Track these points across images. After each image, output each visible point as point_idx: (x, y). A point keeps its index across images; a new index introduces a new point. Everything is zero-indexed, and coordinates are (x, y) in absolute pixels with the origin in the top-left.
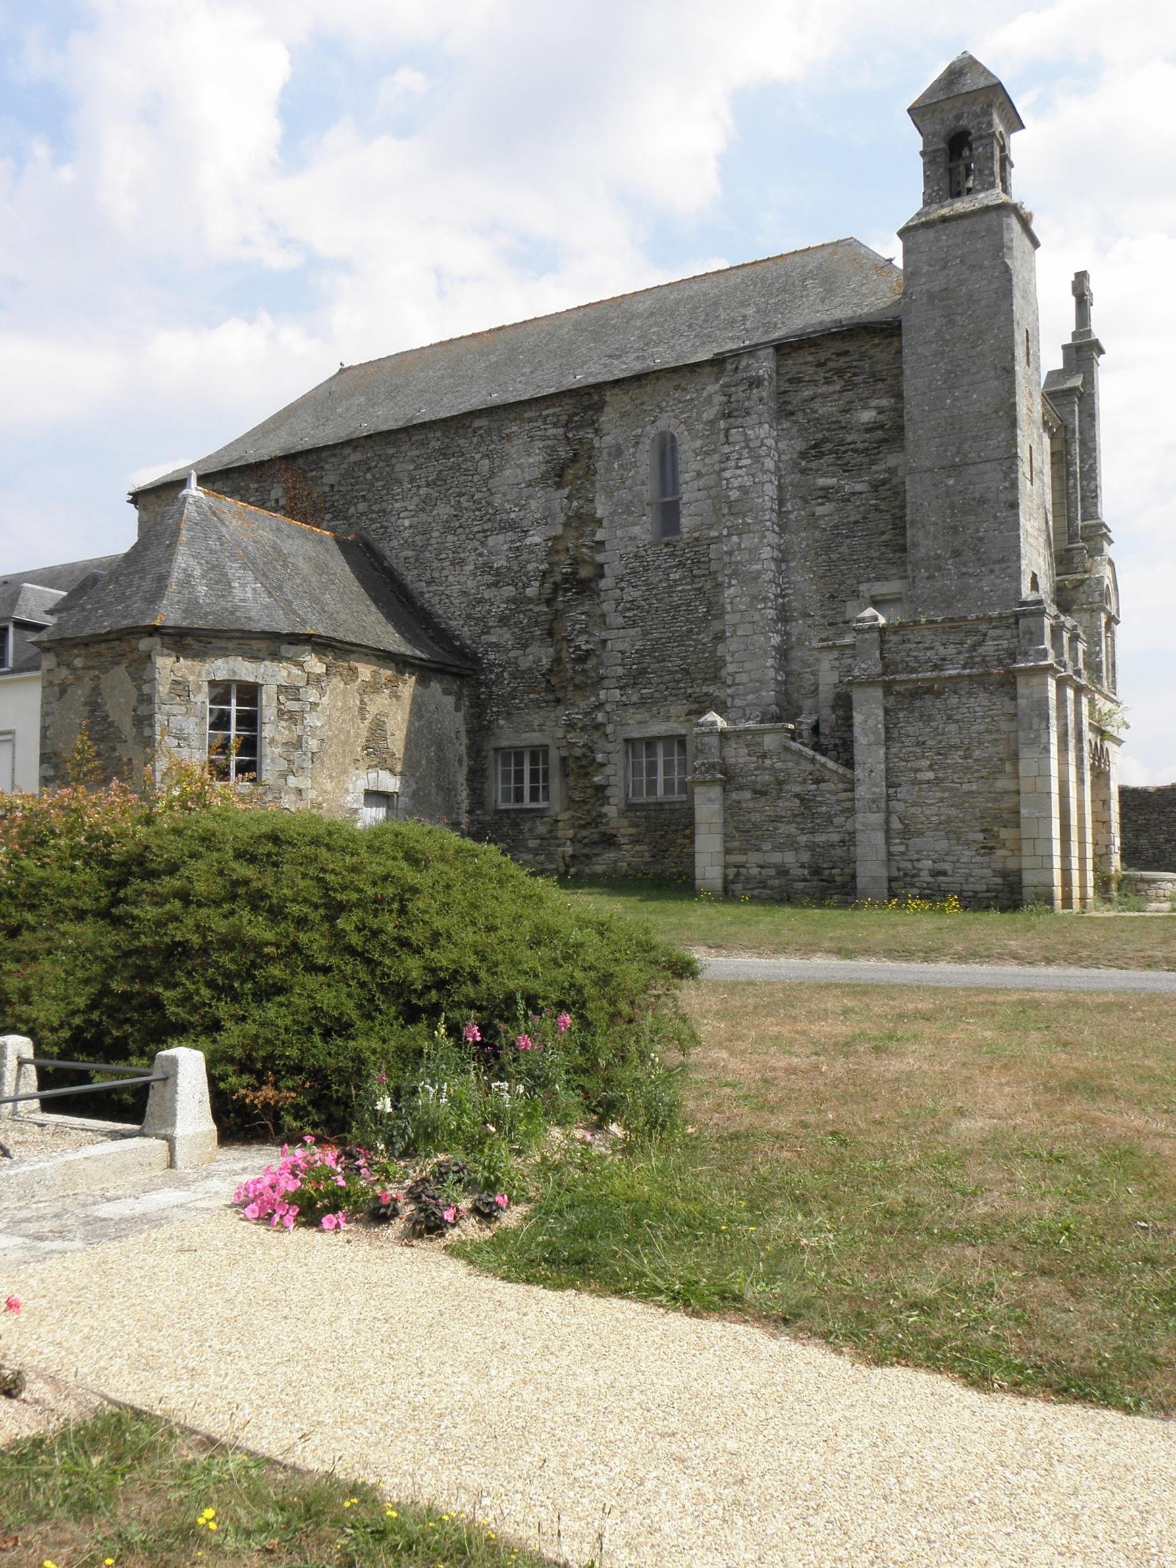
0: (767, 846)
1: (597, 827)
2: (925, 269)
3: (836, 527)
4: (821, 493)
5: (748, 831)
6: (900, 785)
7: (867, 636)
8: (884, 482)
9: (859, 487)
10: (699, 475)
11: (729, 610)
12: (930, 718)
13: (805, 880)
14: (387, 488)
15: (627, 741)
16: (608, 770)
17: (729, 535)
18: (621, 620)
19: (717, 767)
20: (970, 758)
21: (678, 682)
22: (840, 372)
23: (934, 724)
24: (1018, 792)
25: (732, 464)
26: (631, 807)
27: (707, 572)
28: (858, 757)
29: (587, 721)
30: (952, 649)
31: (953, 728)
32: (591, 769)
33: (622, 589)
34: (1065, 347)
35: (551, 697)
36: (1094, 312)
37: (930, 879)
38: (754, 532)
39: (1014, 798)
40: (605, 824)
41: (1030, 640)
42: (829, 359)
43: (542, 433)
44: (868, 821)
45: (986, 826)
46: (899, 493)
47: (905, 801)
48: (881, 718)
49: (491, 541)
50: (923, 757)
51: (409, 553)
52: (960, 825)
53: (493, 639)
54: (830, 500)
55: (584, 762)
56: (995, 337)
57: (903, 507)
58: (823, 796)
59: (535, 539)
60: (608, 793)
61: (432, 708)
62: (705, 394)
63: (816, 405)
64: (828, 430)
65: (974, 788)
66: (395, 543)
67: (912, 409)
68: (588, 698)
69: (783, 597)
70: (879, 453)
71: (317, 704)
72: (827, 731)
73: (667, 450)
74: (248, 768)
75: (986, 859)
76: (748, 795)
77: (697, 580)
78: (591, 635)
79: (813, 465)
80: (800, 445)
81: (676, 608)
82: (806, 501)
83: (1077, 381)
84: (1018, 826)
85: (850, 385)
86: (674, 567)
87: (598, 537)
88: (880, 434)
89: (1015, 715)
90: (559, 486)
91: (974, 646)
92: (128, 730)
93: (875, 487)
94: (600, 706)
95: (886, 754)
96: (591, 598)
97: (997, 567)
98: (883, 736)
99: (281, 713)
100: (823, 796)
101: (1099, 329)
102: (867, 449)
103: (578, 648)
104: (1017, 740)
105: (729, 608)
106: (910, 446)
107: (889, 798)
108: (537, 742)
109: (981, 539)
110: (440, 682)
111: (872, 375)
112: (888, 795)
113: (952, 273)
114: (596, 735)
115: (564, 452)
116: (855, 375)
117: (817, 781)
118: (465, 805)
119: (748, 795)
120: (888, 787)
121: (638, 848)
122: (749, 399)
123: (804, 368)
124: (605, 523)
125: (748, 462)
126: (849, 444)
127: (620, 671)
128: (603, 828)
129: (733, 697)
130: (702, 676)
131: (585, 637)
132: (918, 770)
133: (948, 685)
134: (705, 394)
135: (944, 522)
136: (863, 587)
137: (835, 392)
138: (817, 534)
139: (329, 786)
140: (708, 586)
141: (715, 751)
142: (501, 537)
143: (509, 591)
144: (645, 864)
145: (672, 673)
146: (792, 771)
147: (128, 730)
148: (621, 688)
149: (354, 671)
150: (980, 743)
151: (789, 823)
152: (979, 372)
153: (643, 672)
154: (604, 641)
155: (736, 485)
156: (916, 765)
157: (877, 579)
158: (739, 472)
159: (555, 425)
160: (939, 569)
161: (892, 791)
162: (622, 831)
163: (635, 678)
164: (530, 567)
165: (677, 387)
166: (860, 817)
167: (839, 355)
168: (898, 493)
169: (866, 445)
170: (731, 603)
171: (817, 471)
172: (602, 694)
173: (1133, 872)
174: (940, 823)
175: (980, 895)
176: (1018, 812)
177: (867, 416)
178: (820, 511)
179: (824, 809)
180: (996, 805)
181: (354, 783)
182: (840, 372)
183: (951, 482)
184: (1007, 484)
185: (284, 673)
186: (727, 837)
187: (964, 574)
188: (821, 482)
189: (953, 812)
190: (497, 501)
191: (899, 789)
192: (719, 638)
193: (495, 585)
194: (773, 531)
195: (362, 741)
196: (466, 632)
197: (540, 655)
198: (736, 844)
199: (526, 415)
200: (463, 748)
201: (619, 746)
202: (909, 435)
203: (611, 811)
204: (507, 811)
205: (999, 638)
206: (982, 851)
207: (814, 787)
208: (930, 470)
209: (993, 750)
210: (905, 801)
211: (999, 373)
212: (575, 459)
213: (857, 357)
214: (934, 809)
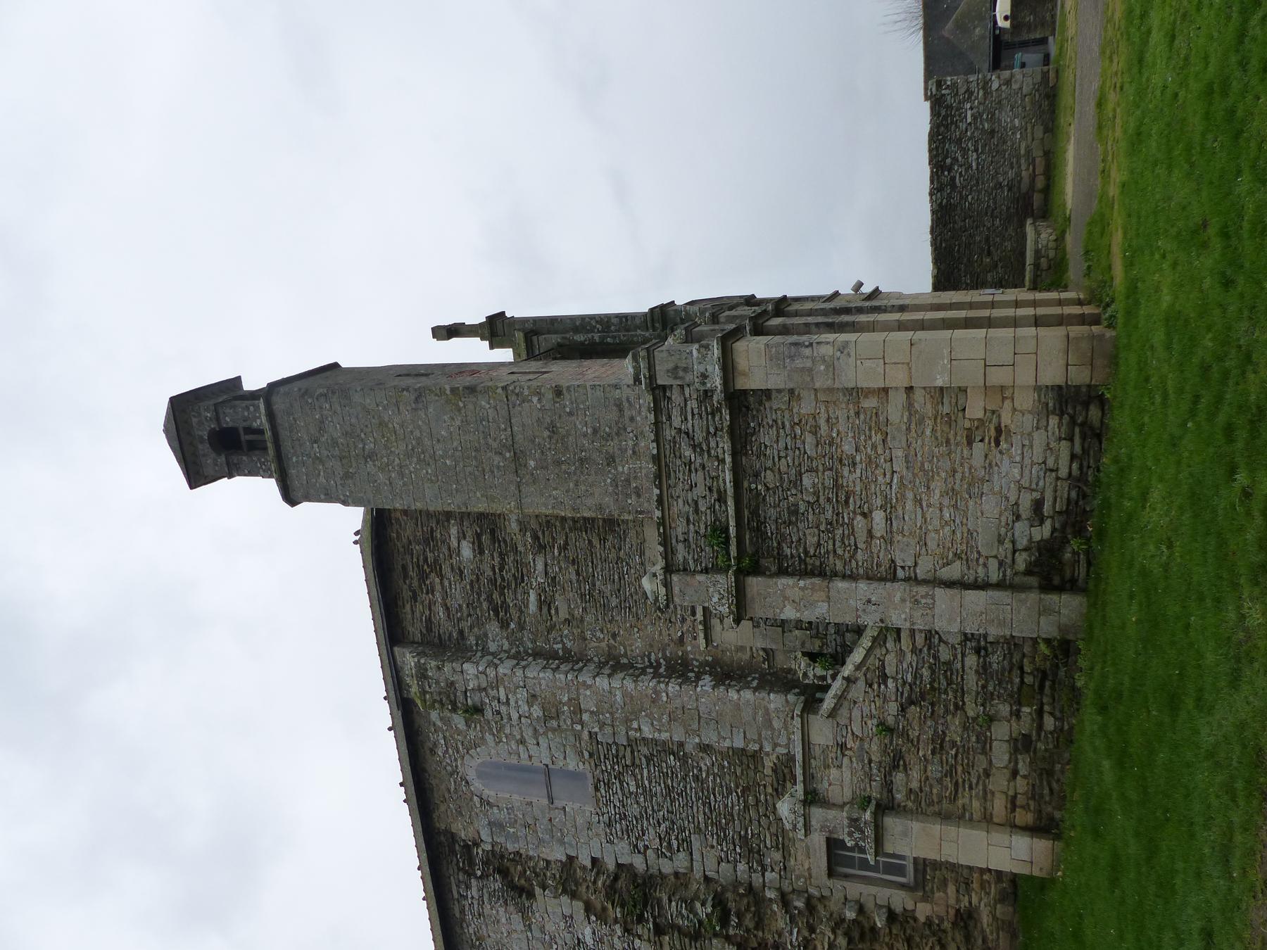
1: (944, 931)
3: (582, 596)
4: (545, 610)
5: (957, 784)
6: (893, 561)
7: (676, 590)
8: (535, 537)
9: (540, 566)
11: (668, 734)
12: (794, 511)
13: (1040, 712)
18: (682, 855)
19: (855, 816)
20: (854, 458)
21: (758, 801)
22: (423, 577)
23: (802, 508)
24: (910, 389)
25: (503, 709)
27: (629, 750)
28: (849, 619)
29: (801, 922)
31: (807, 481)
32: (866, 925)
33: (646, 847)
34: (492, 347)
36: (470, 321)
37: (1048, 525)
38: (578, 694)
39: (919, 396)
40: (941, 920)
41: (685, 370)
42: (410, 586)
43: (475, 902)
46: (548, 523)
47: (917, 556)
48: (790, 581)
50: (851, 525)
52: (958, 476)
55: (856, 935)
57: (564, 519)
58: (905, 671)
60: (899, 910)
62: (439, 723)
63: (453, 604)
64: (479, 595)
65: (900, 453)
67: (452, 504)
69: (659, 665)
70: (505, 541)
72: (818, 643)
75: (1016, 439)
76: (899, 777)
77: (637, 762)
78: (696, 897)
81: (669, 790)
83: (519, 336)
84: (963, 390)
85: (436, 567)
86: (621, 785)
87: (588, 864)
89: (791, 391)
90: (531, 895)
91: (694, 447)
93: (541, 548)
95: (844, 577)
97: (627, 413)
98: (817, 581)
100: (905, 671)
101: (477, 318)
102: (501, 554)
104: (830, 390)
107: (913, 580)
109: (595, 431)
112: (907, 579)
113: (326, 453)
115: (496, 884)
116: (426, 560)
117: (884, 678)
119: (899, 777)
120: (894, 579)
121: (975, 885)
122: (437, 683)
123: (418, 614)
125: (502, 690)
126: (495, 573)
127: (742, 867)
128: (947, 925)
129: (776, 745)
130: (751, 774)
132: (870, 532)
133: (746, 484)
134: (439, 723)
135: (575, 473)
137: (442, 583)
140: (645, 751)
141: (831, 813)
145: (746, 807)
146: (866, 710)
148: (764, 870)
151: (946, 724)
152: (419, 427)
153: (744, 840)
154: (707, 879)
155: (526, 708)
156: (861, 536)
157: (642, 554)
158: (512, 702)
159: (468, 887)
160: (628, 481)
161: (900, 574)
162: (952, 901)
163: (752, 853)
166: (940, 625)
167: (406, 576)
168: (548, 522)
169: (495, 555)
170: (660, 731)
171: (521, 612)
174: (955, 507)
175: (1078, 449)
176: (941, 389)
177: (467, 551)
179: (925, 672)
180: (929, 423)
183: (532, 463)
184: (535, 399)
187: (634, 452)
188: (533, 607)
189: (938, 486)
191: (899, 563)
194: (580, 670)
199: (458, 915)
202: (481, 507)
203: (923, 911)
205: (683, 412)
206: (1004, 445)
207: (890, 683)
210: (917, 556)
211: (420, 406)
213: (408, 557)
214: (932, 513)
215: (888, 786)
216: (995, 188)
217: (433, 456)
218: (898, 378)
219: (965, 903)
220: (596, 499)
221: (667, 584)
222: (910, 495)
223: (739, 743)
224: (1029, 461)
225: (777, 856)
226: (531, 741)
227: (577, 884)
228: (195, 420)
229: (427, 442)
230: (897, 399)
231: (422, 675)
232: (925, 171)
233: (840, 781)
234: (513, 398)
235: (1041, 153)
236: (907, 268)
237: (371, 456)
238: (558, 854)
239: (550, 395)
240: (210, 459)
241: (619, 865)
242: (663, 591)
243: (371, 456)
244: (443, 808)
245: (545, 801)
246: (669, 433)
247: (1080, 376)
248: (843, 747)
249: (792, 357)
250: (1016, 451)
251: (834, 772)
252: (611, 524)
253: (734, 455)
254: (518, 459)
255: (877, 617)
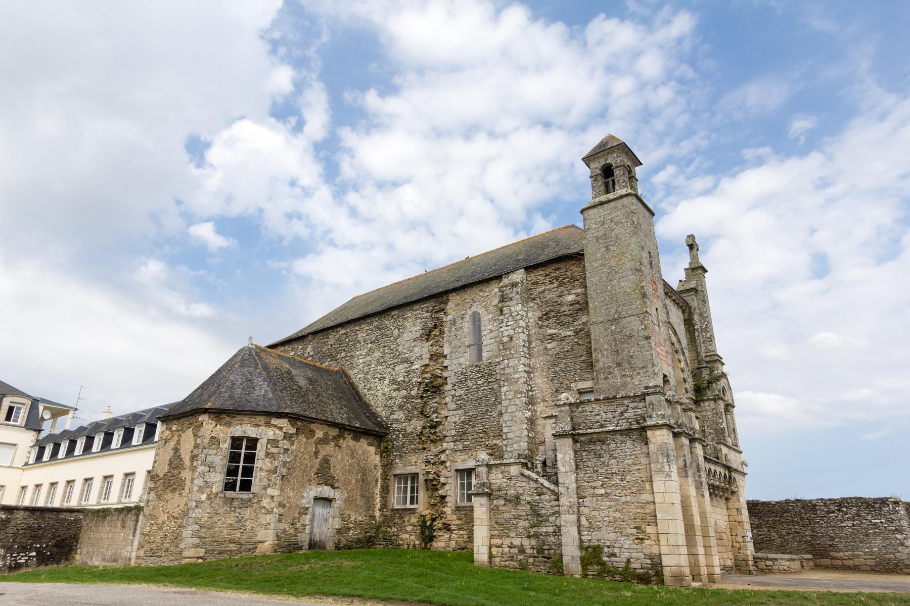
0: (513, 534)
2: (594, 226)
7: (563, 409)
8: (581, 330)
9: (568, 333)
10: (491, 331)
12: (600, 456)
14: (354, 345)
15: (457, 471)
16: (447, 487)
17: (503, 360)
18: (455, 406)
22: (556, 278)
24: (654, 502)
25: (504, 324)
26: (458, 509)
28: (560, 480)
29: (436, 459)
30: (610, 415)
31: (613, 461)
34: (685, 270)
35: (421, 446)
39: (652, 506)
44: (567, 519)
45: (638, 524)
48: (572, 456)
49: (397, 368)
51: (361, 376)
53: (395, 417)
54: (554, 341)
55: (434, 483)
56: (631, 254)
57: (590, 343)
59: (416, 366)
61: (360, 452)
65: (629, 499)
66: (355, 371)
67: (591, 292)
68: (437, 447)
71: (288, 450)
73: (476, 320)
74: (246, 486)
75: (639, 546)
76: (502, 502)
79: (545, 323)
80: (538, 314)
82: (542, 342)
83: (693, 284)
85: (562, 284)
88: (577, 306)
89: (648, 454)
90: (427, 340)
91: (622, 413)
92: (187, 462)
93: (577, 333)
94: (443, 451)
96: (440, 395)
97: (641, 371)
98: (574, 467)
99: (267, 455)
103: (432, 420)
105: (503, 397)
106: (591, 311)
108: (414, 471)
109: (631, 357)
110: (367, 439)
111: (572, 278)
114: (442, 467)
115: (430, 324)
118: (378, 506)
121: (461, 532)
124: (448, 357)
127: (454, 432)
129: (506, 446)
131: (436, 415)
132: (595, 488)
136: (573, 385)
138: (548, 358)
139: (291, 494)
141: (485, 476)
142: (401, 366)
143: (404, 393)
144: (465, 542)
147: (187, 462)
149: (313, 432)
150: (630, 471)
153: (464, 433)
156: (593, 484)
157: (580, 380)
159: (427, 312)
161: (581, 500)
163: (461, 436)
164: (413, 380)
165: (481, 290)
166: (563, 517)
172: (445, 444)
173: (760, 555)
177: (571, 298)
178: (549, 346)
180: (642, 511)
181: (308, 493)
182: (556, 278)
183: (613, 328)
185: (272, 433)
186: (491, 528)
189: (618, 515)
190: (400, 348)
192: (501, 414)
193: (397, 390)
195: (314, 470)
196: (382, 412)
197: (417, 424)
198: (496, 532)
200: (379, 474)
201: (453, 474)
202: (591, 305)
203: (448, 510)
204: (397, 510)
205: (635, 408)
208: (603, 322)
209: (637, 475)
212: (435, 327)
215: (498, 498)
216: (830, 537)
217: (611, 280)
218: (658, 499)
219: (453, 528)
220: (603, 360)
221: (564, 404)
222: (612, 504)
223: (505, 430)
224: (626, 551)
225: (460, 447)
226: (492, 335)
227: (435, 360)
228: (615, 155)
229: (618, 276)
230: (649, 498)
231: (515, 285)
232: (837, 495)
233: (497, 478)
234: (642, 316)
235: (857, 563)
236: (750, 489)
237: (607, 249)
238: (446, 351)
239: (645, 334)
240: (598, 165)
241: (446, 378)
242: (562, 403)
243: (607, 249)
244: (458, 297)
245: (467, 344)
246: (626, 402)
247: (667, 572)
248: (510, 479)
249: (662, 454)
250: (634, 546)
251: (500, 476)
252: (591, 365)
253: (620, 430)
254: (615, 321)
255: (562, 491)
